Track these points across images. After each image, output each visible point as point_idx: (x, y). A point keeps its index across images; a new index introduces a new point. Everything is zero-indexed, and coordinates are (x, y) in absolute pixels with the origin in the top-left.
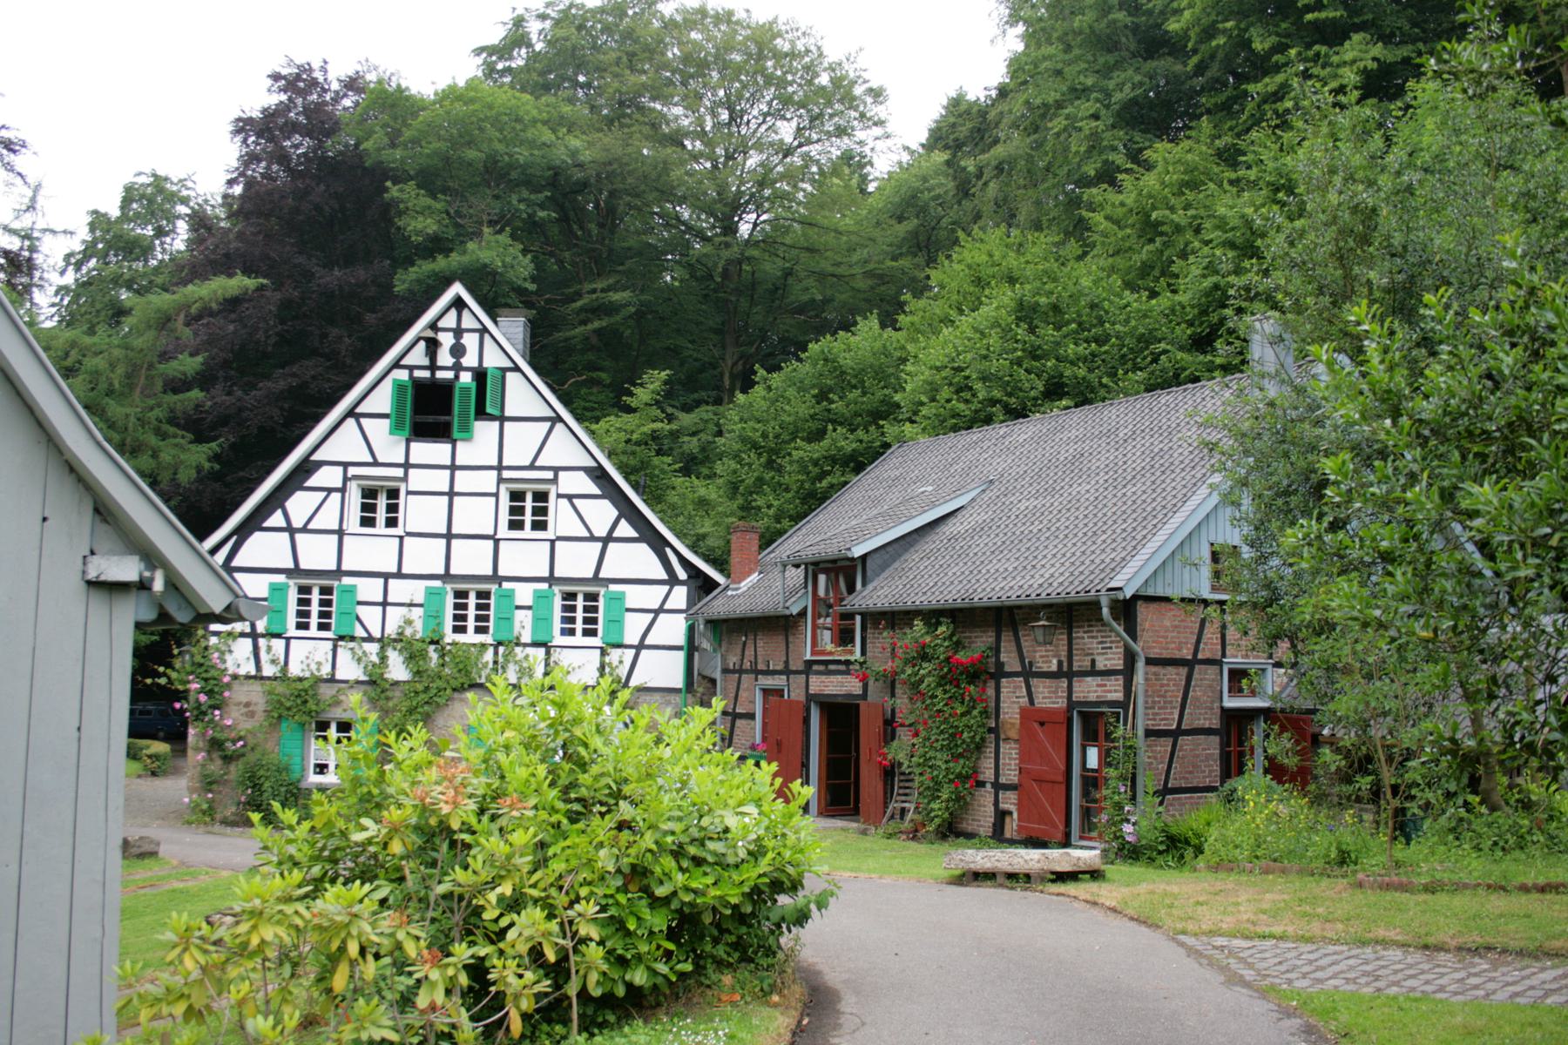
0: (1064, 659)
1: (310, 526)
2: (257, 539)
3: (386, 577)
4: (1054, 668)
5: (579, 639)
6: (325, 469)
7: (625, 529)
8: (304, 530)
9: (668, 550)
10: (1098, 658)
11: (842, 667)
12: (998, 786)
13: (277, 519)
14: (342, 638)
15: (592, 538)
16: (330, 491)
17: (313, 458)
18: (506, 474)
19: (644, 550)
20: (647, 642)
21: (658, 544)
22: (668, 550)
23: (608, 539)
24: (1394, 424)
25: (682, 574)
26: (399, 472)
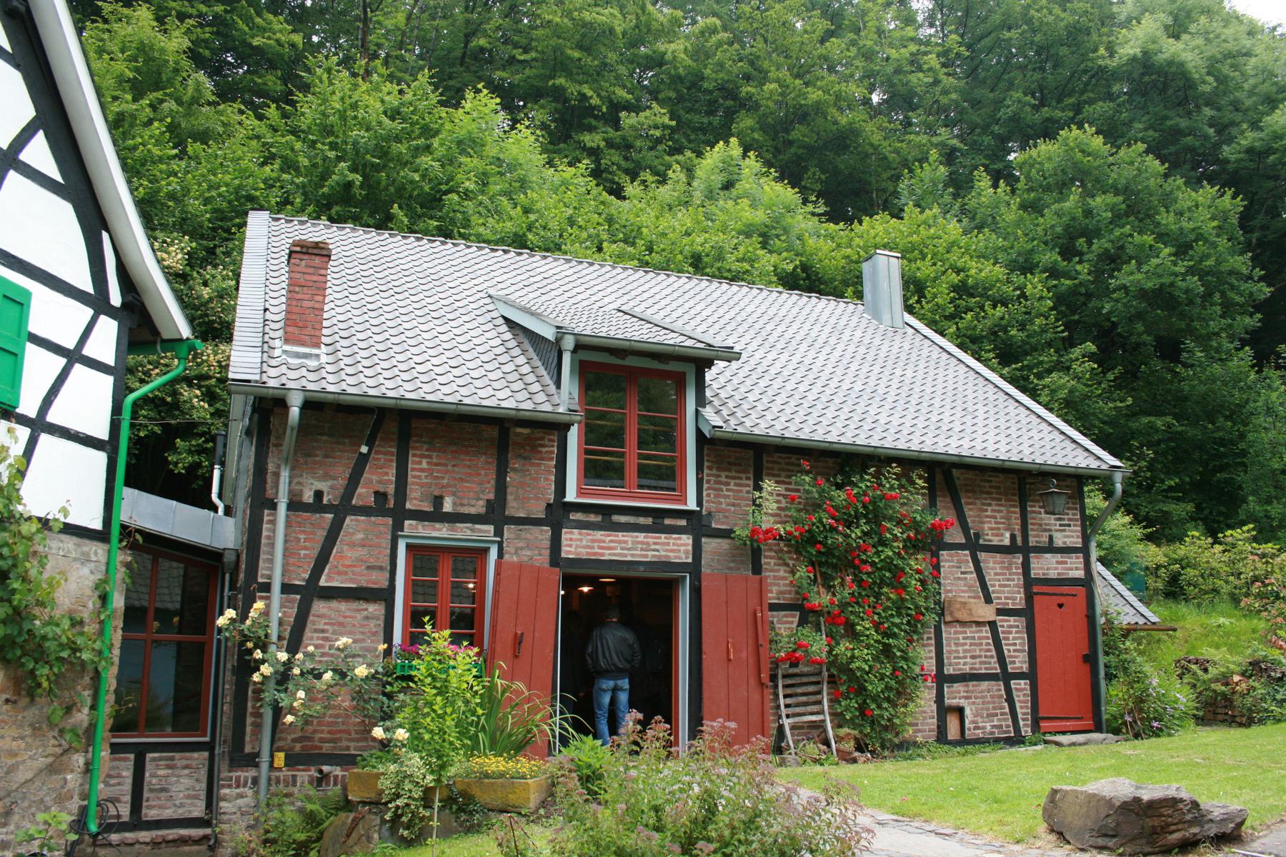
0: (1018, 533)
4: (1007, 542)
7: (39, 153)
9: (105, 235)
10: (1055, 535)
11: (649, 521)
12: (942, 679)
19: (63, 215)
21: (94, 220)
22: (105, 235)
24: (872, 729)
25: (116, 299)
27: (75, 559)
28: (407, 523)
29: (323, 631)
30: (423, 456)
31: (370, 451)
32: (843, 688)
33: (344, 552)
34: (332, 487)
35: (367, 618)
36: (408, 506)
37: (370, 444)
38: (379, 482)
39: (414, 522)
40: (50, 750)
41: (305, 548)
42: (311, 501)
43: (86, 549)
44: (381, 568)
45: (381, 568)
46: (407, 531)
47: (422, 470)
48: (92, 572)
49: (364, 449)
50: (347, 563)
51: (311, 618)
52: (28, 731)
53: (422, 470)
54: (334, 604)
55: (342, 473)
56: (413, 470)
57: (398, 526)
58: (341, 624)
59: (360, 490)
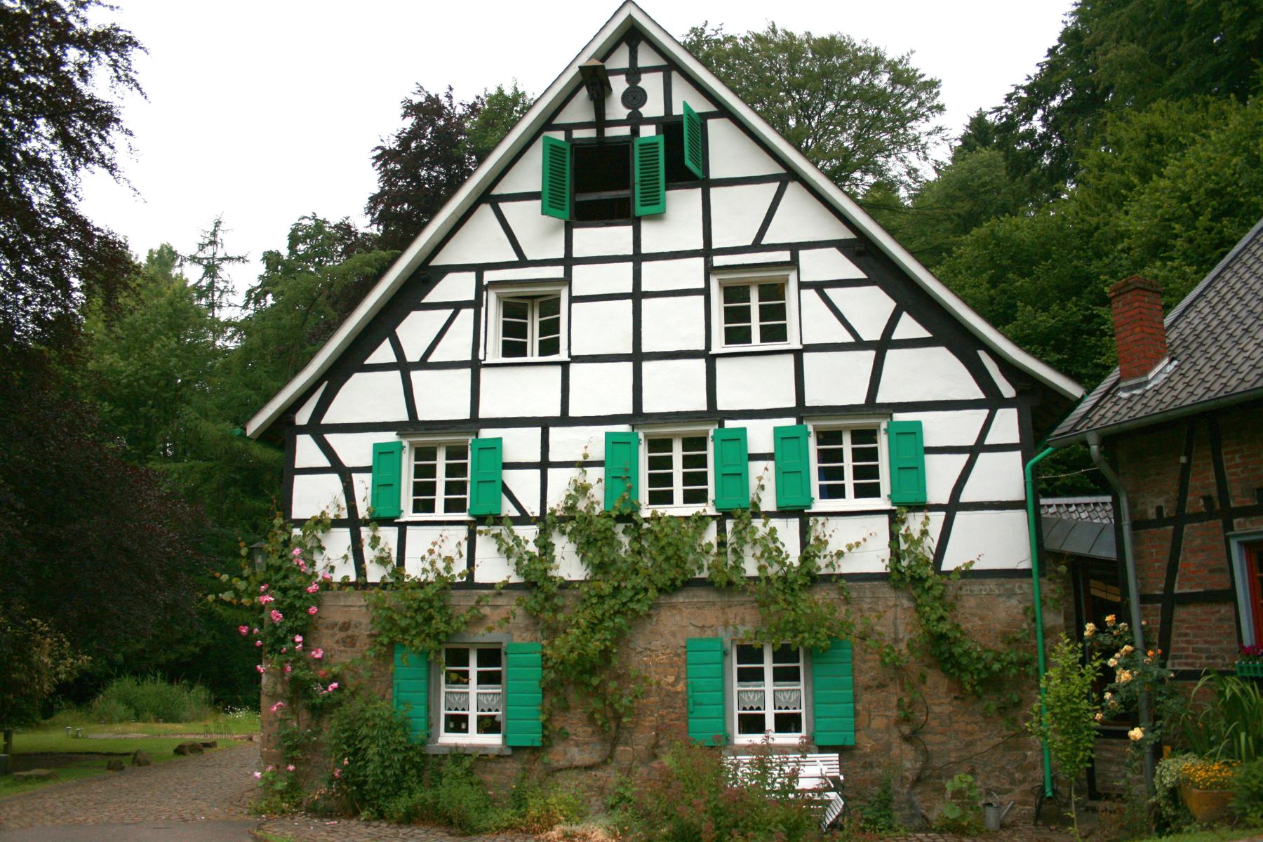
2: (358, 383)
7: (908, 327)
8: (423, 364)
9: (983, 355)
13: (384, 353)
15: (859, 344)
18: (718, 261)
21: (965, 345)
22: (983, 355)
23: (883, 345)
25: (1008, 391)
26: (558, 272)
27: (999, 595)
28: (1235, 521)
29: (1186, 635)
30: (1234, 452)
31: (1189, 461)
32: (1057, 710)
33: (1190, 561)
34: (1167, 501)
35: (1220, 620)
36: (1232, 505)
37: (1188, 454)
38: (1203, 487)
39: (1242, 520)
40: (1005, 732)
41: (1158, 561)
42: (1154, 517)
43: (1008, 586)
44: (1222, 570)
45: (1222, 570)
46: (1237, 530)
47: (1237, 466)
48: (1020, 602)
49: (1183, 460)
50: (1192, 569)
51: (1175, 624)
52: (980, 719)
53: (1237, 466)
54: (1192, 609)
55: (1172, 485)
56: (1228, 468)
57: (1228, 526)
58: (1199, 628)
59: (1189, 498)
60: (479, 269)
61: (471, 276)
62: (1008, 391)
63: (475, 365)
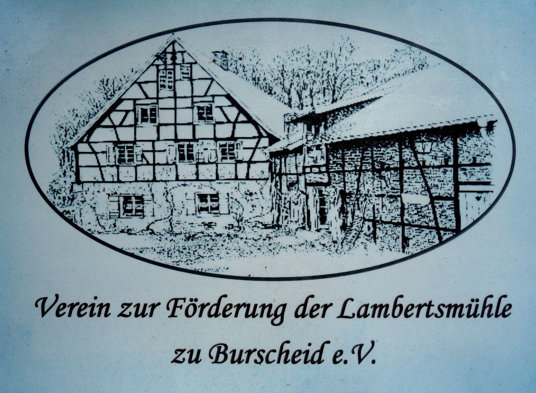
1: (124, 124)
2: (98, 131)
3: (153, 141)
5: (228, 161)
6: (125, 102)
7: (242, 118)
8: (121, 125)
9: (260, 128)
13: (107, 122)
14: (194, 127)
15: (229, 121)
16: (127, 112)
17: (122, 98)
18: (195, 99)
20: (252, 151)
23: (236, 122)
26: (155, 101)
60: (135, 100)
61: (132, 102)
62: (264, 134)
63: (135, 126)
